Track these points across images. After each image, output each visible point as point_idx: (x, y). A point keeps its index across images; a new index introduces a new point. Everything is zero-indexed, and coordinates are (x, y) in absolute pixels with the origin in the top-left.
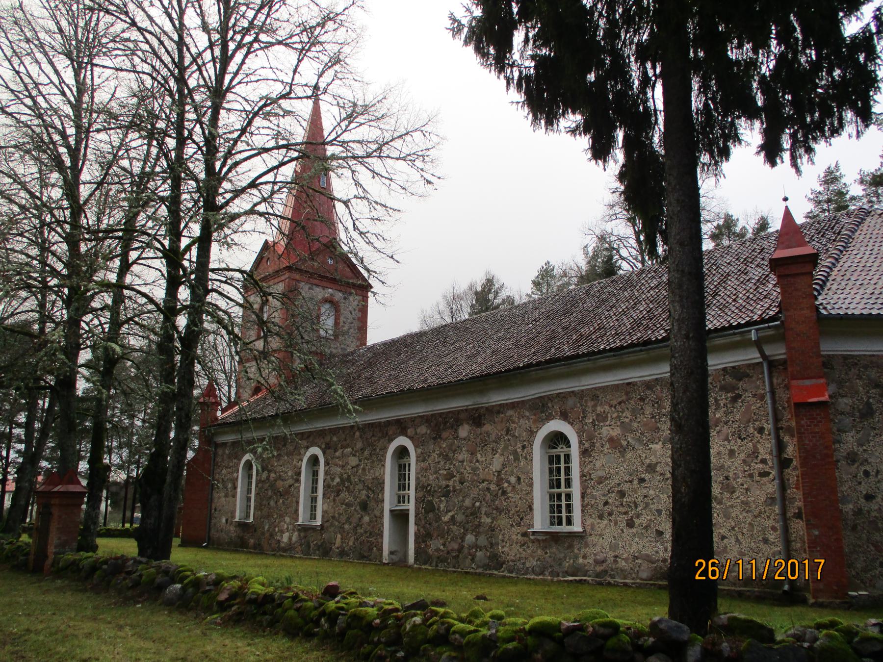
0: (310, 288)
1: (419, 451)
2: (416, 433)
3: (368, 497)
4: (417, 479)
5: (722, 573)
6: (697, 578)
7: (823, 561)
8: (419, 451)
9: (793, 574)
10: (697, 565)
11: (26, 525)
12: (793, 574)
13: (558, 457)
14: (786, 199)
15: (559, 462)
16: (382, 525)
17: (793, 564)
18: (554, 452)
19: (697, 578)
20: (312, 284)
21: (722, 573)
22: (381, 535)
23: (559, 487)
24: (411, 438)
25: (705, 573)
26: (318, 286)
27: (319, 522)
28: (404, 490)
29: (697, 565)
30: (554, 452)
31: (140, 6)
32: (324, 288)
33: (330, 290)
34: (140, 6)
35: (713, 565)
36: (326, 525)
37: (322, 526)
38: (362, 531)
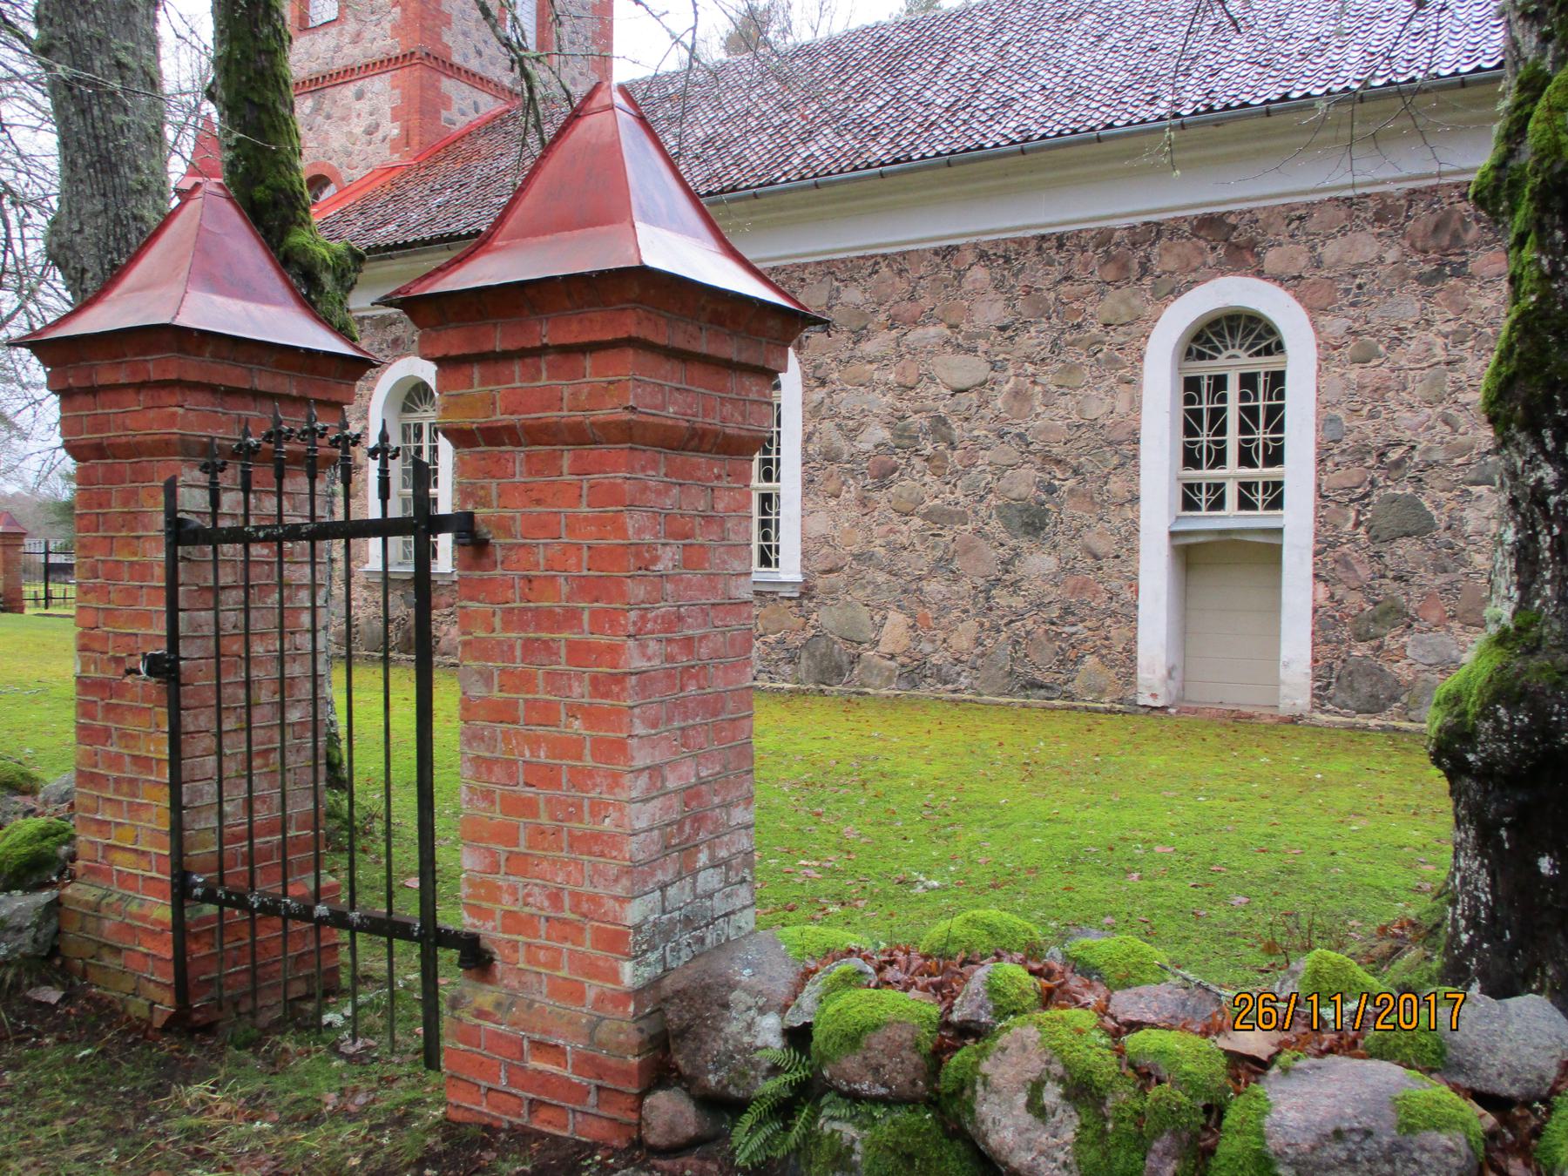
1: (1336, 325)
2: (1318, 264)
3: (1051, 490)
4: (1326, 422)
8: (1336, 325)
11: (865, 1165)
13: (419, 428)
15: (419, 436)
16: (1133, 583)
22: (1128, 615)
24: (1288, 281)
27: (789, 569)
30: (1204, 369)
36: (821, 582)
37: (807, 591)
38: (1018, 602)
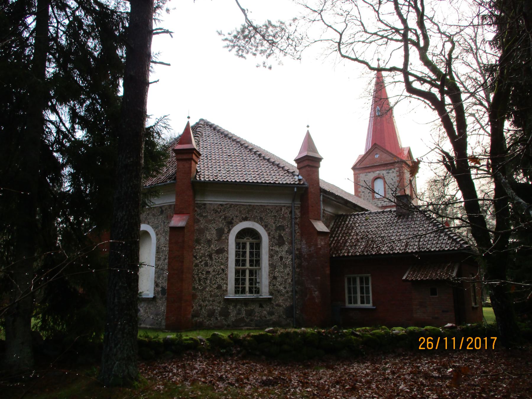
0: (366, 175)
5: (435, 346)
6: (420, 348)
7: (496, 338)
9: (478, 346)
10: (420, 340)
12: (478, 346)
14: (308, 126)
17: (478, 340)
18: (241, 241)
19: (420, 348)
20: (366, 173)
21: (435, 346)
23: (244, 265)
25: (425, 345)
26: (369, 172)
28: (253, 276)
29: (420, 340)
31: (3, 310)
32: (373, 172)
33: (378, 172)
34: (3, 310)
35: (430, 340)
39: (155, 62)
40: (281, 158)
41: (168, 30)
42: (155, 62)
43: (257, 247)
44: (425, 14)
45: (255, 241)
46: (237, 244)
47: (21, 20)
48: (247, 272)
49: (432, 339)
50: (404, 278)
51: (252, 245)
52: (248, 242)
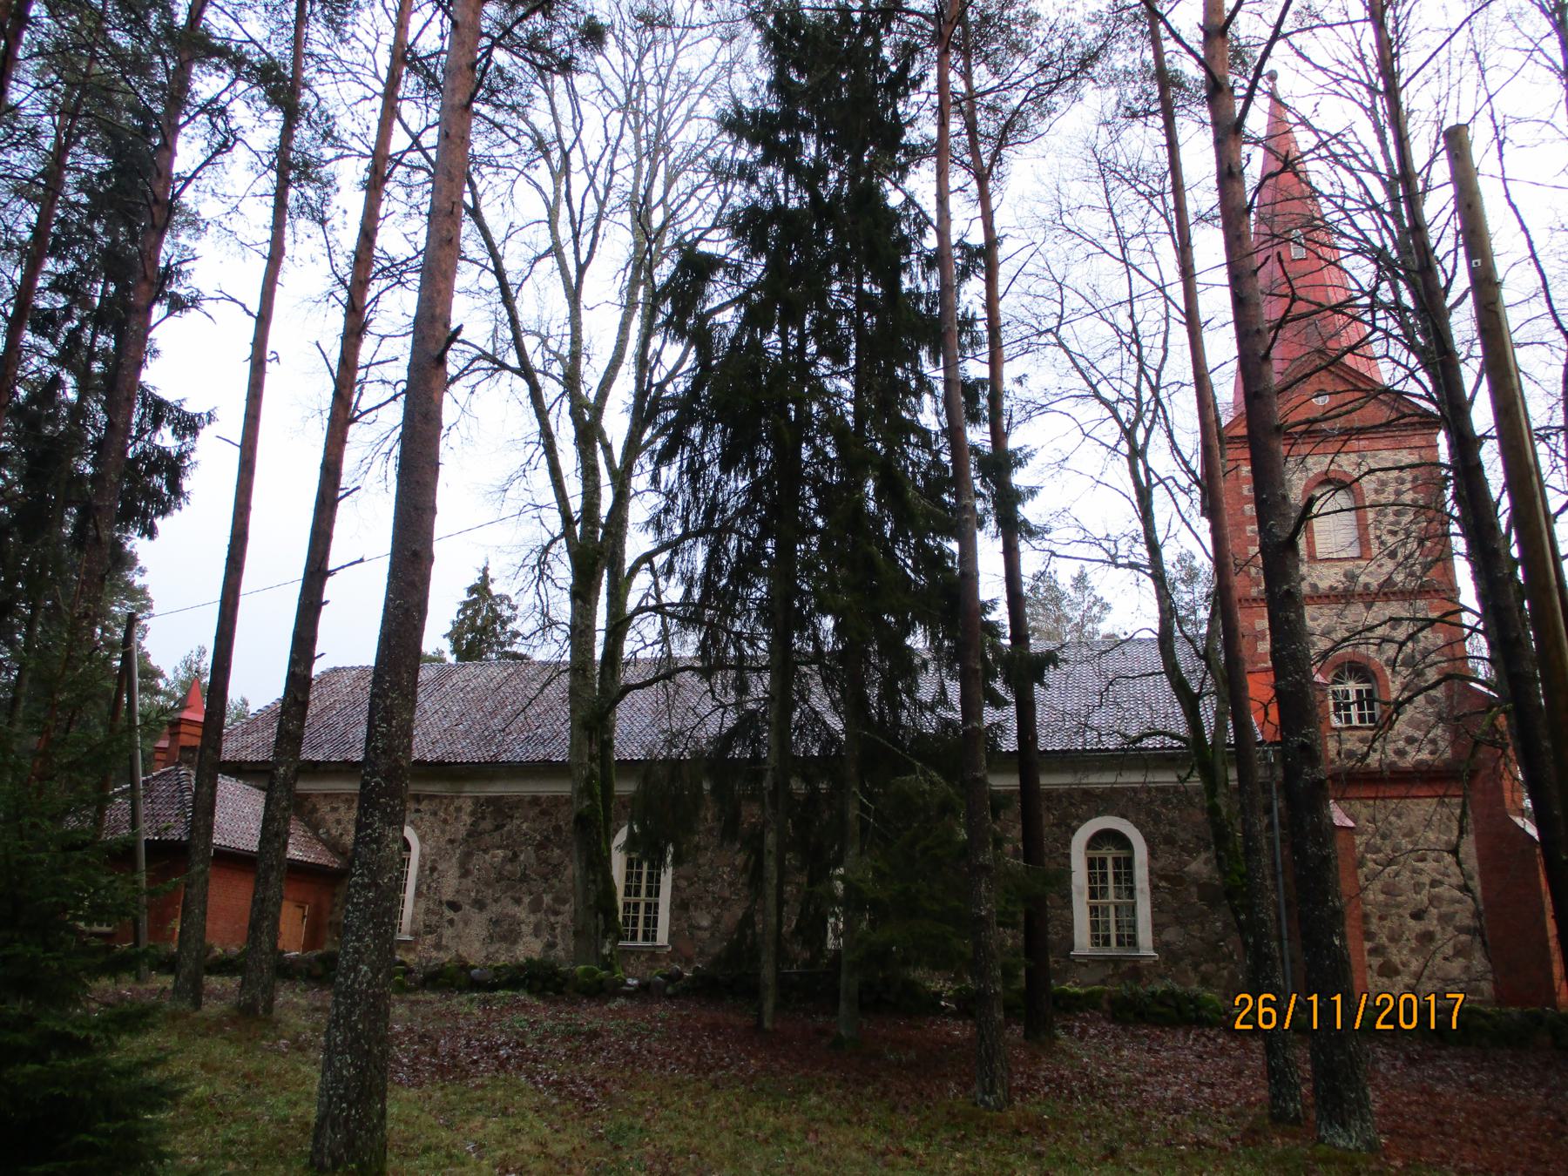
5: (1281, 1021)
9: (1408, 1020)
12: (1408, 1020)
18: (1097, 854)
21: (1281, 1021)
25: (1252, 1018)
30: (1097, 854)
35: (1267, 1003)
39: (1519, 345)
40: (378, 633)
41: (472, 590)
42: (1519, 345)
43: (1126, 866)
44: (253, 321)
45: (1122, 854)
46: (1091, 864)
47: (899, 613)
48: (1112, 909)
49: (1273, 998)
50: (1532, 830)
51: (1116, 861)
52: (1109, 853)
